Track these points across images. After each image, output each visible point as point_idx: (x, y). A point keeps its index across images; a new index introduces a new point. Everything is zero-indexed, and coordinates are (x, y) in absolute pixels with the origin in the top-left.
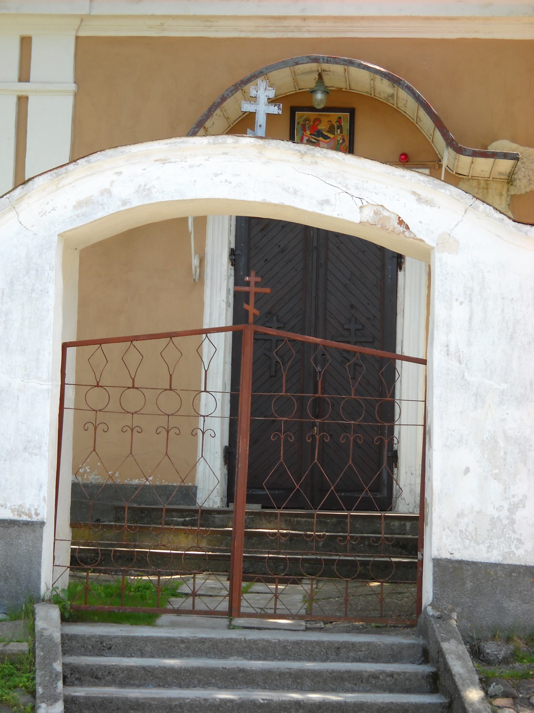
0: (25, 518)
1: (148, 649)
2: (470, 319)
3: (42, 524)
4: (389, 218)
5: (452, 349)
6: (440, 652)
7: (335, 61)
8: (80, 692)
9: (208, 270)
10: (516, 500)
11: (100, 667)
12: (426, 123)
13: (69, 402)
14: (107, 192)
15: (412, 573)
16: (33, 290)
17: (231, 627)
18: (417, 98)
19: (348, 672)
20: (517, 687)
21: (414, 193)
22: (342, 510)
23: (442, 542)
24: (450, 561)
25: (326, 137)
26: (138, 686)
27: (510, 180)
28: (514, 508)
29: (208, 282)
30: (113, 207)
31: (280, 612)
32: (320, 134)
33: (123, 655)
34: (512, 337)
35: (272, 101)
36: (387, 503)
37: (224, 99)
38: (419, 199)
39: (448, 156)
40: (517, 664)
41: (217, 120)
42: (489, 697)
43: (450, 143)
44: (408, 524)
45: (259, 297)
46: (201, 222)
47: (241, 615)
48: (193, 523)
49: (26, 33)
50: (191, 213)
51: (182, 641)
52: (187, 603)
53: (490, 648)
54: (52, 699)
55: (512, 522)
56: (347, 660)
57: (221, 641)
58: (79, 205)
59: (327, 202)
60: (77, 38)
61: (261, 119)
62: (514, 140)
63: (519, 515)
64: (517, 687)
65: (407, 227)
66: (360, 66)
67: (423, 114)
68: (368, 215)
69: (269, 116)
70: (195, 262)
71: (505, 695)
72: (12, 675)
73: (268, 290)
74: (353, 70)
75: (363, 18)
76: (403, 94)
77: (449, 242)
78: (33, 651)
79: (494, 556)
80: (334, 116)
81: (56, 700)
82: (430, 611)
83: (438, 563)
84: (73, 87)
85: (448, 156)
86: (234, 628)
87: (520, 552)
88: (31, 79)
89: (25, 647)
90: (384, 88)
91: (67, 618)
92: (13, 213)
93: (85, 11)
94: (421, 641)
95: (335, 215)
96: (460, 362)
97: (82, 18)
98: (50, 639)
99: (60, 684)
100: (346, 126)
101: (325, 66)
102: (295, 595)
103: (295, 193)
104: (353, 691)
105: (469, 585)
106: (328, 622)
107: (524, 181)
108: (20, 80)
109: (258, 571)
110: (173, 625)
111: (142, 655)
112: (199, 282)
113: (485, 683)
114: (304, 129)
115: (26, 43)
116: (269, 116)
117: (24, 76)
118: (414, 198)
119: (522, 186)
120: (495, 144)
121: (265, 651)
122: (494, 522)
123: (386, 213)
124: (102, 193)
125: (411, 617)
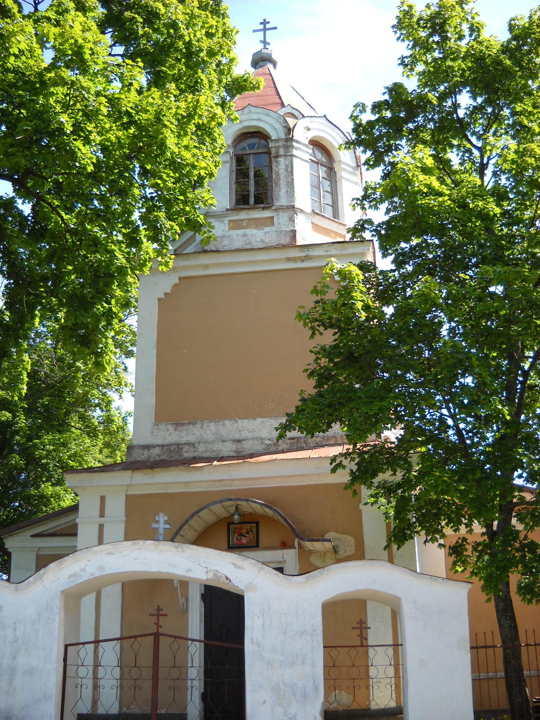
2: (264, 625)
4: (220, 577)
5: (255, 640)
10: (291, 716)
14: (84, 570)
16: (49, 619)
21: (233, 563)
25: (245, 536)
29: (190, 610)
30: (86, 577)
34: (285, 633)
38: (236, 566)
41: (188, 532)
49: (103, 494)
59: (190, 570)
60: (126, 495)
62: (337, 532)
65: (230, 581)
68: (210, 576)
77: (251, 587)
80: (249, 526)
84: (124, 519)
88: (106, 515)
92: (40, 582)
93: (129, 483)
95: (194, 576)
96: (259, 647)
97: (128, 486)
100: (254, 530)
101: (238, 502)
103: (174, 566)
108: (100, 517)
112: (185, 611)
114: (234, 533)
115: (103, 498)
117: (102, 515)
118: (233, 566)
123: (219, 574)
124: (81, 570)
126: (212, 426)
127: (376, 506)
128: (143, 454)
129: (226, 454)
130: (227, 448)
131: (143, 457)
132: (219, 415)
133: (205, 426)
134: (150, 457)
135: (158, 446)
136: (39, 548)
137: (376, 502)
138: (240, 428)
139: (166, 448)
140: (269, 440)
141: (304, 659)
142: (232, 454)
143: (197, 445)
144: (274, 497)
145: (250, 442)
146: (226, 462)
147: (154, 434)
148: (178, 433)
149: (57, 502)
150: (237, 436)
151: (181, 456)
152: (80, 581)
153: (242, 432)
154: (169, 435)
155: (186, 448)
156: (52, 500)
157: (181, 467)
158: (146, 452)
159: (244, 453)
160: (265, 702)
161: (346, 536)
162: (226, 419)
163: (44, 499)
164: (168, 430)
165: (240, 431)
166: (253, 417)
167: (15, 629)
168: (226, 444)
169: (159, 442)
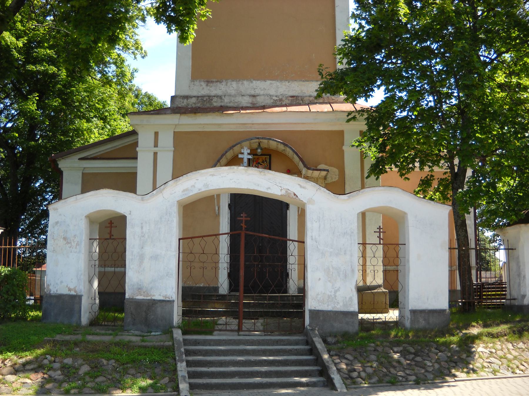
0: (167, 299)
1: (212, 343)
3: (174, 301)
4: (290, 193)
5: (314, 238)
6: (313, 342)
7: (265, 139)
8: (190, 358)
9: (221, 211)
11: (196, 350)
12: (296, 159)
13: (181, 259)
14: (193, 186)
15: (302, 315)
17: (239, 335)
18: (294, 151)
19: (281, 349)
20: (340, 352)
21: (299, 185)
22: (276, 293)
23: (313, 303)
24: (315, 310)
25: (261, 164)
26: (210, 356)
27: (325, 178)
28: (336, 292)
29: (221, 215)
30: (195, 191)
31: (255, 330)
32: (259, 163)
33: (203, 345)
35: (248, 154)
36: (286, 291)
37: (226, 152)
38: (301, 186)
39: (304, 171)
40: (339, 344)
41: (224, 161)
42: (331, 356)
43: (305, 166)
44: (294, 298)
45: (246, 221)
46: (218, 196)
47: (242, 331)
48: (219, 300)
49: (156, 131)
50: (215, 193)
51: (224, 340)
52: (224, 327)
53: (329, 339)
54: (182, 361)
55: (335, 296)
56: (280, 345)
57: (237, 340)
58: (184, 191)
59: (269, 188)
61: (246, 160)
62: (326, 164)
63: (338, 294)
64: (340, 352)
66: (273, 140)
67: (295, 156)
68: (283, 192)
69: (249, 160)
70: (217, 208)
71: (336, 355)
72: (167, 353)
73: (249, 219)
74: (271, 142)
75: (273, 124)
76: (288, 149)
77: (311, 201)
78: (173, 344)
79: (330, 308)
81: (183, 361)
82: (308, 328)
83: (311, 311)
84: (173, 149)
85: (304, 171)
86: (240, 335)
87: (338, 306)
89: (170, 343)
90: (281, 147)
91: (184, 333)
92: (161, 194)
93: (177, 123)
94: (305, 338)
97: (176, 125)
98: (179, 340)
99: (184, 356)
100: (268, 160)
101: (261, 140)
102: (260, 323)
103: (258, 185)
104: (283, 356)
105: (321, 318)
106: (272, 332)
107: (330, 178)
109: (250, 316)
110: (219, 335)
111: (210, 345)
112: (218, 216)
113: (329, 351)
115: (156, 134)
116: (249, 160)
117: (156, 145)
118: (299, 186)
119: (329, 180)
120: (320, 166)
121: (252, 343)
122: (329, 297)
123: (289, 192)
124: (192, 187)
125: (301, 330)
126: (234, 84)
127: (359, 148)
128: (183, 102)
129: (245, 105)
130: (245, 101)
131: (183, 105)
132: (239, 76)
133: (229, 84)
134: (188, 104)
135: (195, 97)
136: (84, 168)
137: (359, 145)
138: (255, 87)
139: (200, 98)
140: (276, 96)
141: (345, 251)
142: (249, 105)
143: (223, 97)
144: (289, 138)
145: (262, 97)
146: (248, 111)
147: (191, 88)
148: (208, 88)
149: (88, 134)
150: (253, 93)
151: (212, 104)
152: (191, 194)
153: (256, 90)
154: (201, 89)
155: (215, 99)
156: (85, 132)
157: (217, 113)
158: (185, 101)
159: (258, 105)
160: (320, 279)
161: (332, 168)
162: (244, 80)
163: (79, 132)
164: (201, 85)
165: (254, 89)
166: (264, 79)
167: (142, 227)
168: (245, 98)
169: (195, 93)
